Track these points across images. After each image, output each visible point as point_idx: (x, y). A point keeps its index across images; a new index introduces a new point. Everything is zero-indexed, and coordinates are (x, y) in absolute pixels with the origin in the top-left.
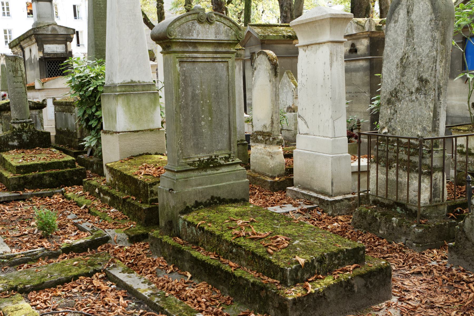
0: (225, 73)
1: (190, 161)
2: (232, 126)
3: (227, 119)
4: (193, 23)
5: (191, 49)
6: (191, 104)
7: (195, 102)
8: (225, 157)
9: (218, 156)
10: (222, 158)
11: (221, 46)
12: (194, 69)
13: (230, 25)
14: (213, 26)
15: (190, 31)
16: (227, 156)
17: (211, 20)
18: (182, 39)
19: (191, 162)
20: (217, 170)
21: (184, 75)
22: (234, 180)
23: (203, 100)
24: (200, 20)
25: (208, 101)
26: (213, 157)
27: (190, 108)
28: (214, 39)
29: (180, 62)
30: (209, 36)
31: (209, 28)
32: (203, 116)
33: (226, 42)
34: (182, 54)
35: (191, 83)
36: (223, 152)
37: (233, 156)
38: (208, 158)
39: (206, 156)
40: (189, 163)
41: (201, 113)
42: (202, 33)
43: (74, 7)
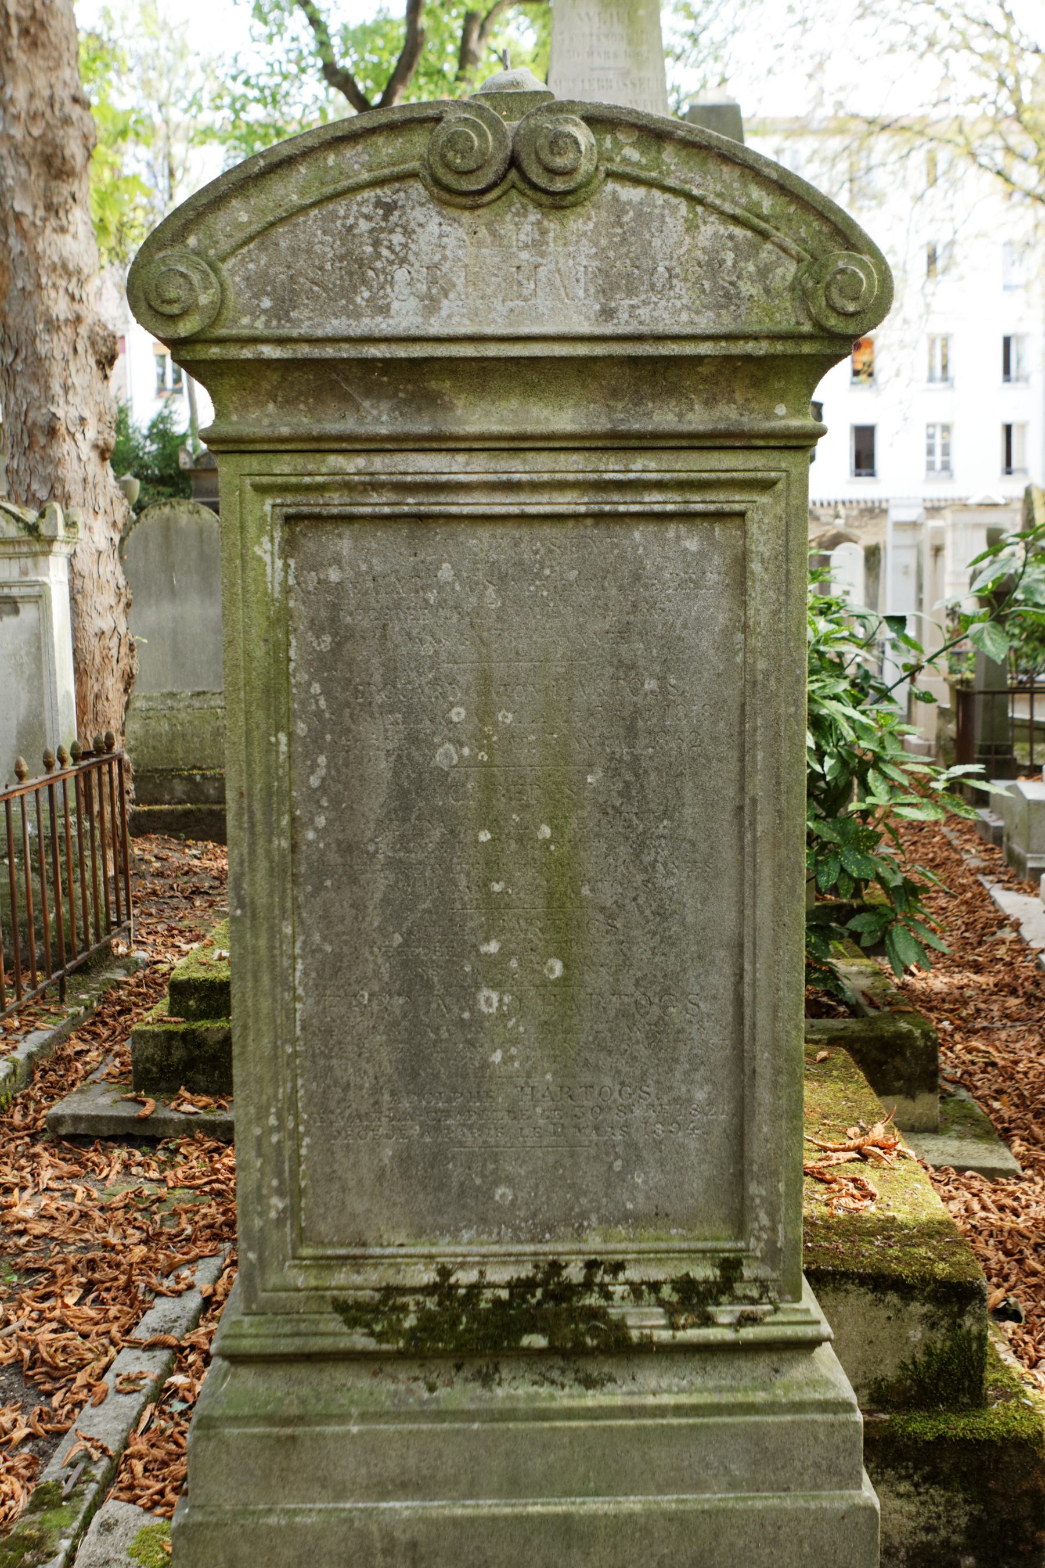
1: (361, 1283)
3: (720, 981)
4: (389, 208)
5: (380, 418)
6: (383, 847)
7: (420, 834)
8: (686, 1286)
9: (618, 1267)
10: (655, 1287)
11: (674, 391)
12: (422, 576)
13: (753, 208)
14: (580, 223)
15: (356, 269)
16: (704, 1272)
17: (553, 172)
18: (281, 341)
19: (365, 1295)
20: (589, 1383)
21: (331, 622)
22: (733, 1485)
23: (494, 824)
24: (449, 179)
25: (546, 831)
26: (575, 1273)
27: (380, 881)
28: (585, 328)
30: (543, 303)
31: (538, 246)
32: (493, 947)
33: (705, 349)
34: (300, 462)
35: (389, 681)
36: (676, 1238)
37: (764, 1286)
38: (526, 1271)
39: (504, 1259)
40: (350, 1296)
41: (477, 919)
42: (472, 281)
43: (1007, 341)
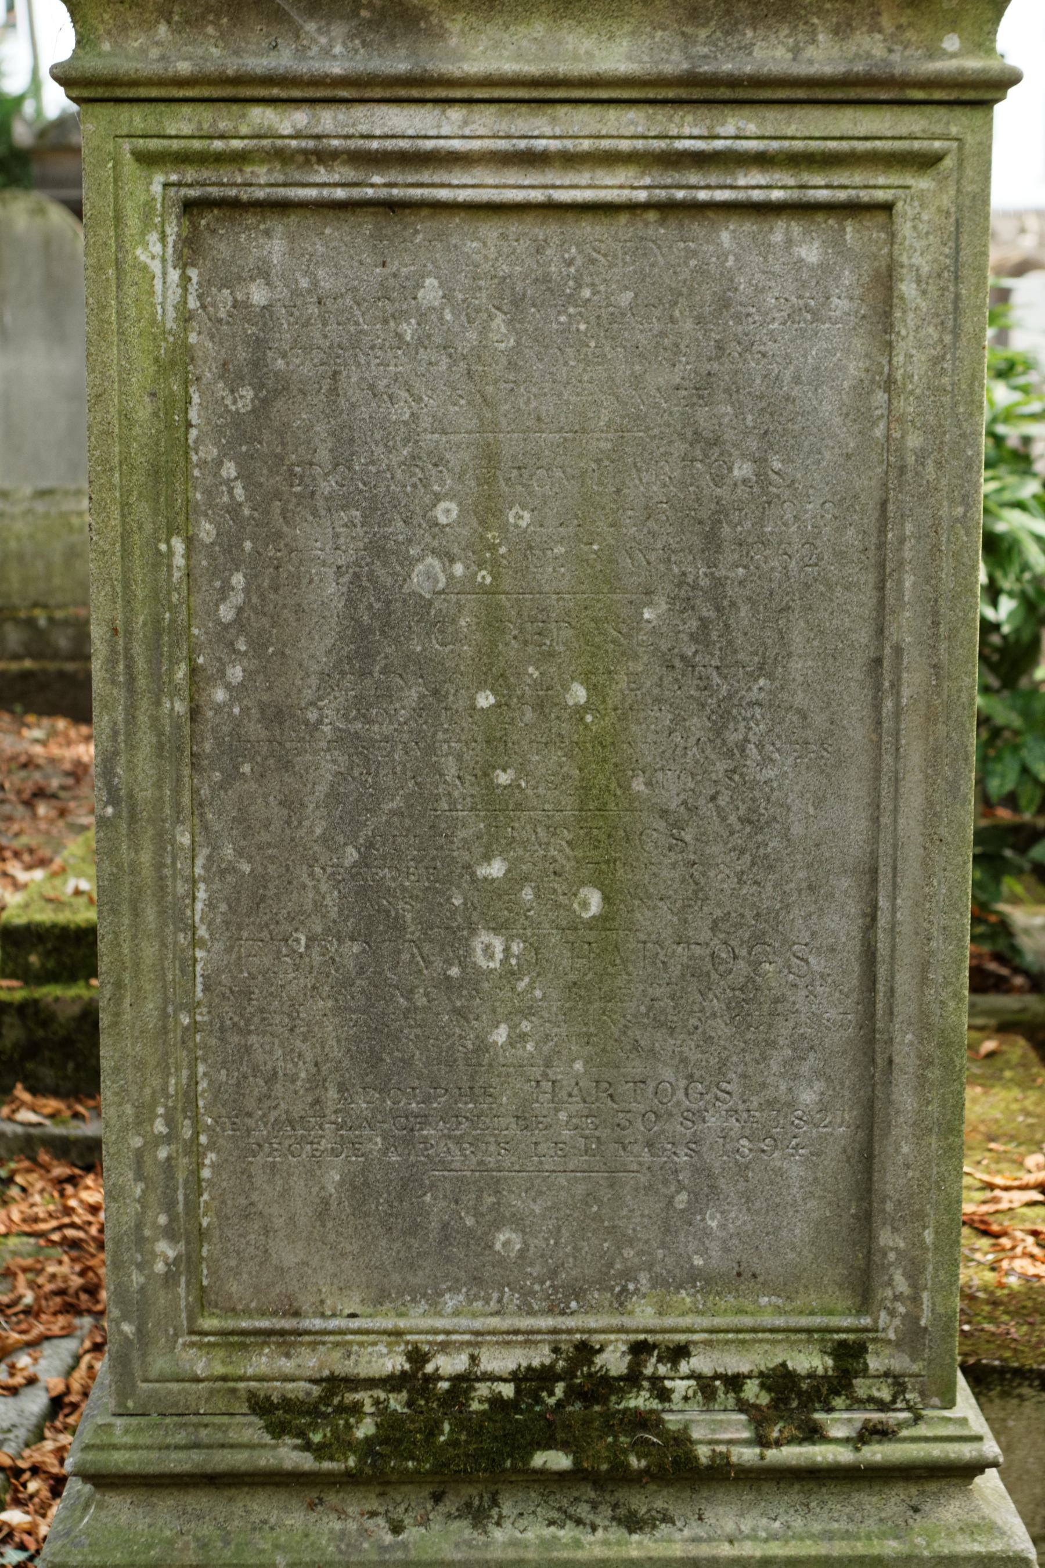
0: (841, 352)
1: (294, 1371)
2: (905, 1009)
3: (841, 925)
6: (330, 714)
7: (387, 694)
8: (781, 1382)
9: (680, 1352)
10: (734, 1382)
16: (809, 1361)
19: (298, 1389)
20: (633, 1523)
21: (253, 367)
25: (579, 694)
26: (614, 1360)
27: (325, 767)
29: (190, 207)
32: (496, 869)
34: (206, 117)
36: (767, 1311)
37: (898, 1381)
38: (540, 1357)
39: (508, 1338)
40: (276, 1390)
